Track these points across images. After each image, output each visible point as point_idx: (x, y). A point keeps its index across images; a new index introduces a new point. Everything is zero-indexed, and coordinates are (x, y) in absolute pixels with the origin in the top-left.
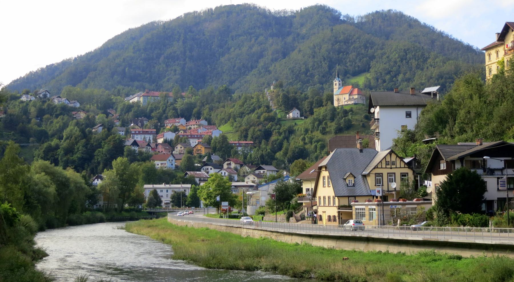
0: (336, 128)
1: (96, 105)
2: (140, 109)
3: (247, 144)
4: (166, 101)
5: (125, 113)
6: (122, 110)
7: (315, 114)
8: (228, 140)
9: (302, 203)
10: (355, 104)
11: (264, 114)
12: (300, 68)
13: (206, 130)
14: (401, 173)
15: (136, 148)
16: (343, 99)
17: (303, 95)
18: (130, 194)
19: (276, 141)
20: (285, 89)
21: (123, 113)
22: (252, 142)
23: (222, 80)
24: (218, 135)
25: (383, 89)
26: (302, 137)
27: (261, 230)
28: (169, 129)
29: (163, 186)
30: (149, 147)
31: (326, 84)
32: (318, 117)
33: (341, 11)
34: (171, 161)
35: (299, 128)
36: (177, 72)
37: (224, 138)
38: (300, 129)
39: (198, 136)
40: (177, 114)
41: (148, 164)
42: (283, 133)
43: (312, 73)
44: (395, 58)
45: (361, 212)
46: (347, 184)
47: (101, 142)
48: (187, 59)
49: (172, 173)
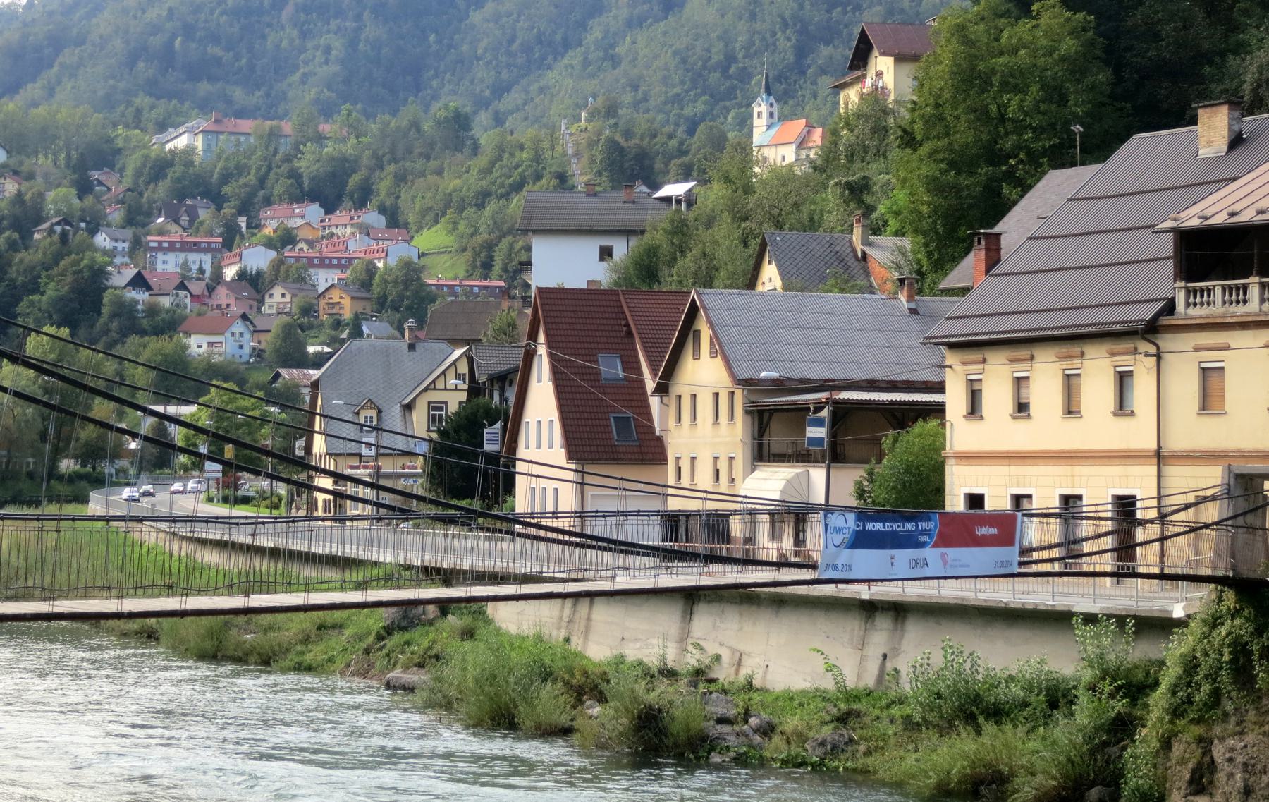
1: (63, 155)
2: (191, 171)
3: (486, 287)
4: (271, 149)
5: (148, 184)
6: (138, 173)
12: (708, 51)
15: (141, 296)
21: (141, 181)
22: (502, 284)
23: (472, 82)
30: (182, 293)
34: (238, 335)
36: (334, 53)
39: (343, 261)
43: (745, 68)
47: (39, 277)
48: (366, 15)
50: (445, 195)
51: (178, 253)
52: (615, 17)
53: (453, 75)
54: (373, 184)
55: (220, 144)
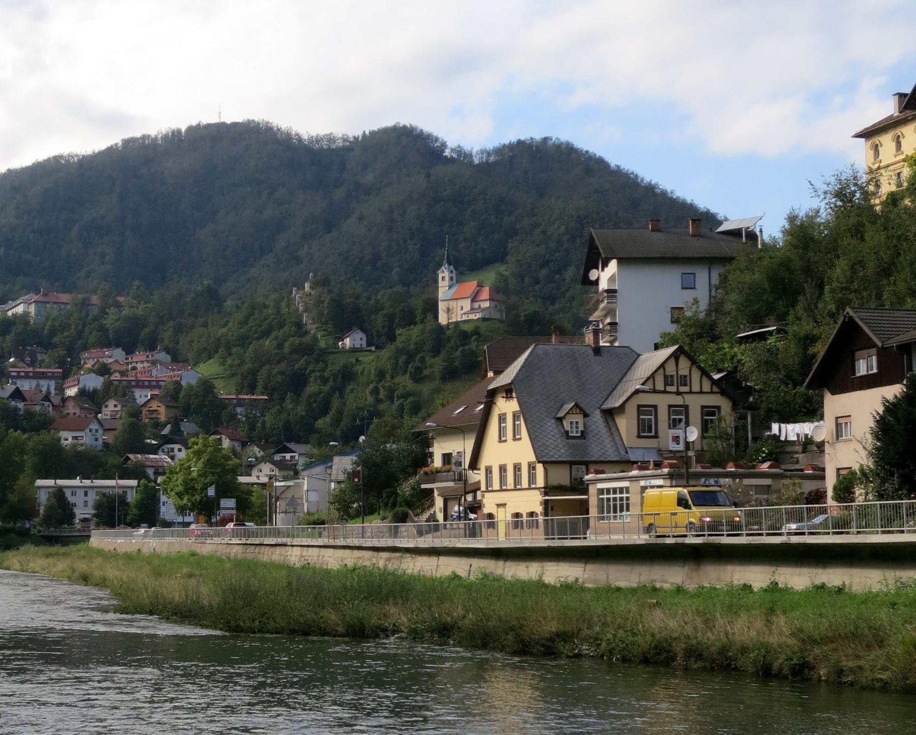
2: (29, 328)
4: (84, 313)
9: (432, 490)
10: (484, 319)
11: (292, 339)
13: (169, 371)
14: (703, 407)
15: (21, 405)
16: (459, 308)
17: (372, 302)
22: (266, 397)
24: (194, 382)
26: (371, 386)
27: (344, 547)
28: (89, 369)
29: (76, 482)
30: (47, 404)
31: (416, 285)
33: (445, 139)
34: (94, 431)
35: (364, 369)
37: (207, 386)
38: (366, 372)
45: (615, 499)
46: (567, 432)
51: (31, 380)
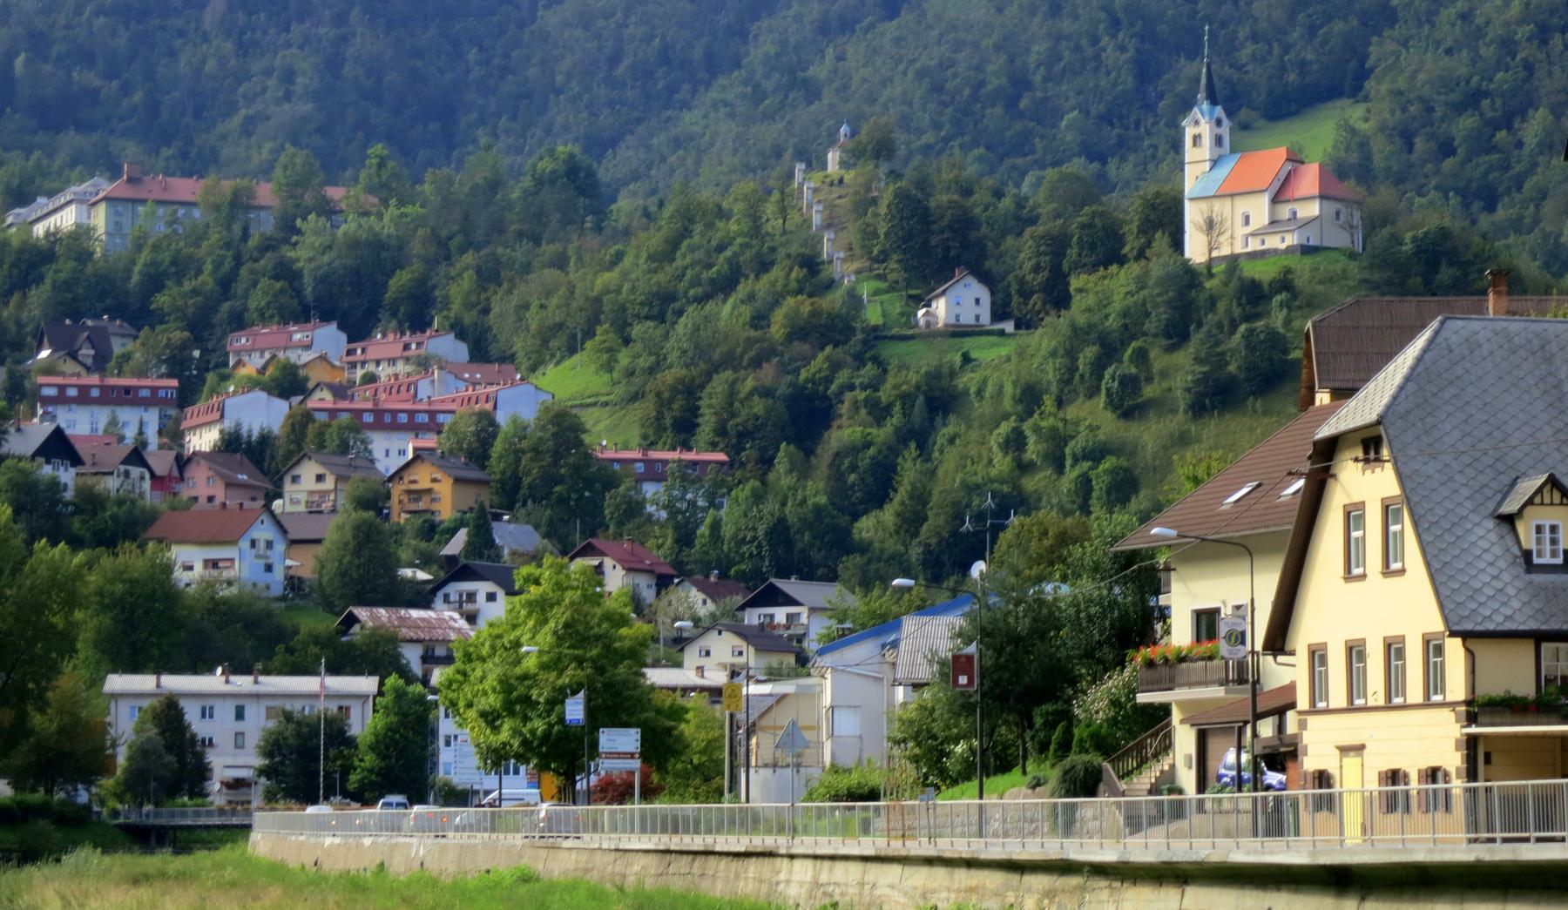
0: (1197, 382)
2: (89, 269)
3: (695, 463)
4: (237, 229)
7: (1078, 302)
8: (587, 439)
9: (1164, 711)
10: (1306, 250)
11: (791, 301)
12: (979, 68)
13: (462, 385)
15: (67, 476)
16: (1239, 220)
17: (1007, 203)
18: (22, 717)
19: (855, 450)
20: (909, 172)
22: (722, 457)
24: (529, 415)
25: (1437, 188)
26: (1005, 428)
27: (929, 861)
28: (250, 379)
29: (214, 682)
30: (135, 471)
31: (1123, 159)
32: (1095, 318)
34: (262, 545)
35: (985, 381)
36: (300, 80)
38: (990, 390)
40: (295, 302)
41: (131, 560)
42: (897, 408)
43: (1046, 99)
44: (1507, 24)
46: (1527, 555)
49: (269, 614)
50: (587, 299)
52: (798, 18)
53: (513, 118)
54: (434, 287)
55: (140, 221)
